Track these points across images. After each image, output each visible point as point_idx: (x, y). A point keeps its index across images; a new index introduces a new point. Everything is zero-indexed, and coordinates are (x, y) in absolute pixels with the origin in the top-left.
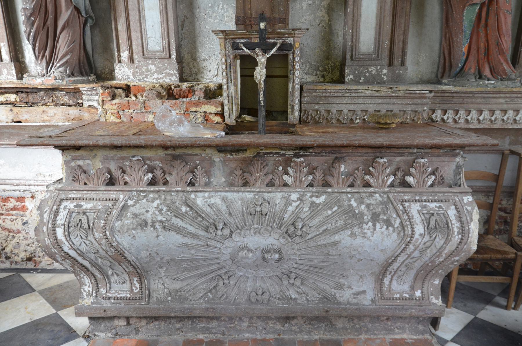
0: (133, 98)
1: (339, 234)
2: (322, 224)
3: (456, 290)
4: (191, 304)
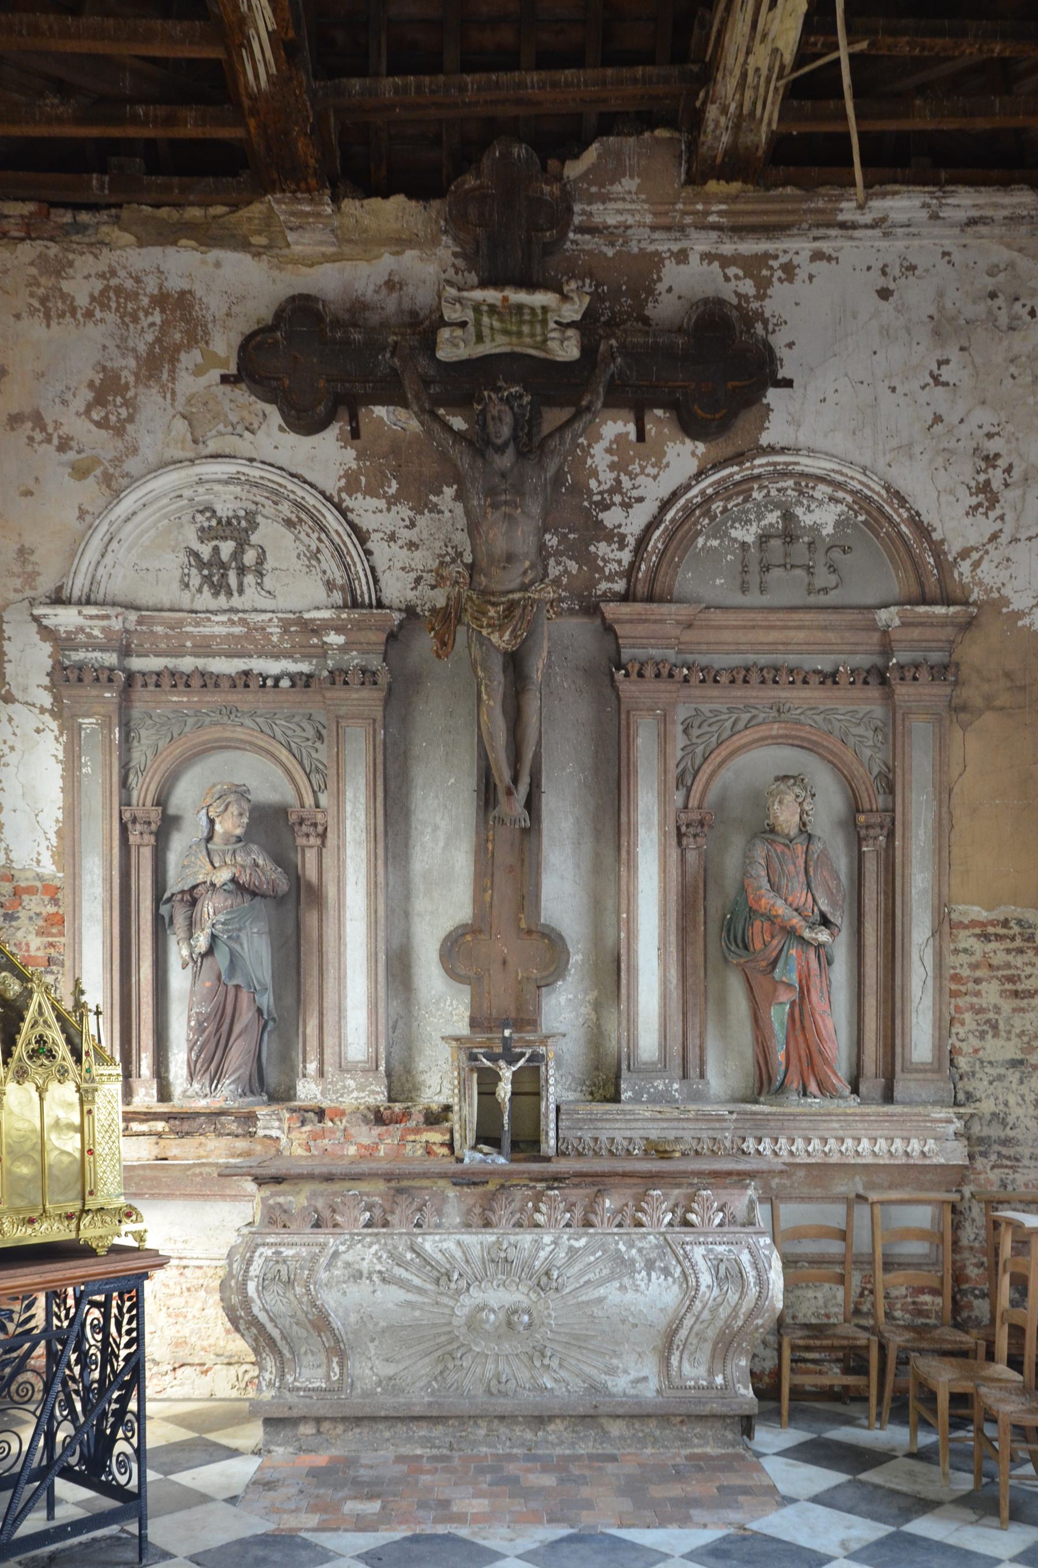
0: (330, 1124)
2: (582, 1273)
3: (790, 1400)
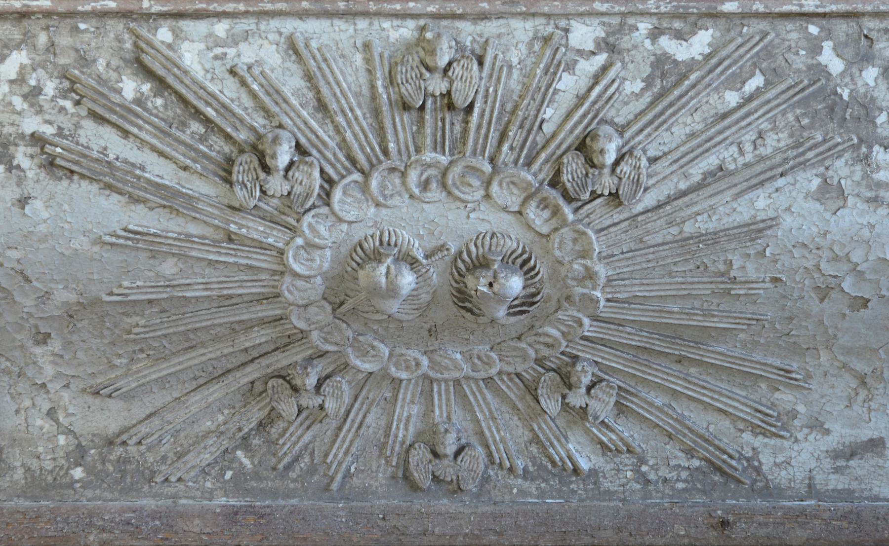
1: (770, 187)
4: (168, 497)
